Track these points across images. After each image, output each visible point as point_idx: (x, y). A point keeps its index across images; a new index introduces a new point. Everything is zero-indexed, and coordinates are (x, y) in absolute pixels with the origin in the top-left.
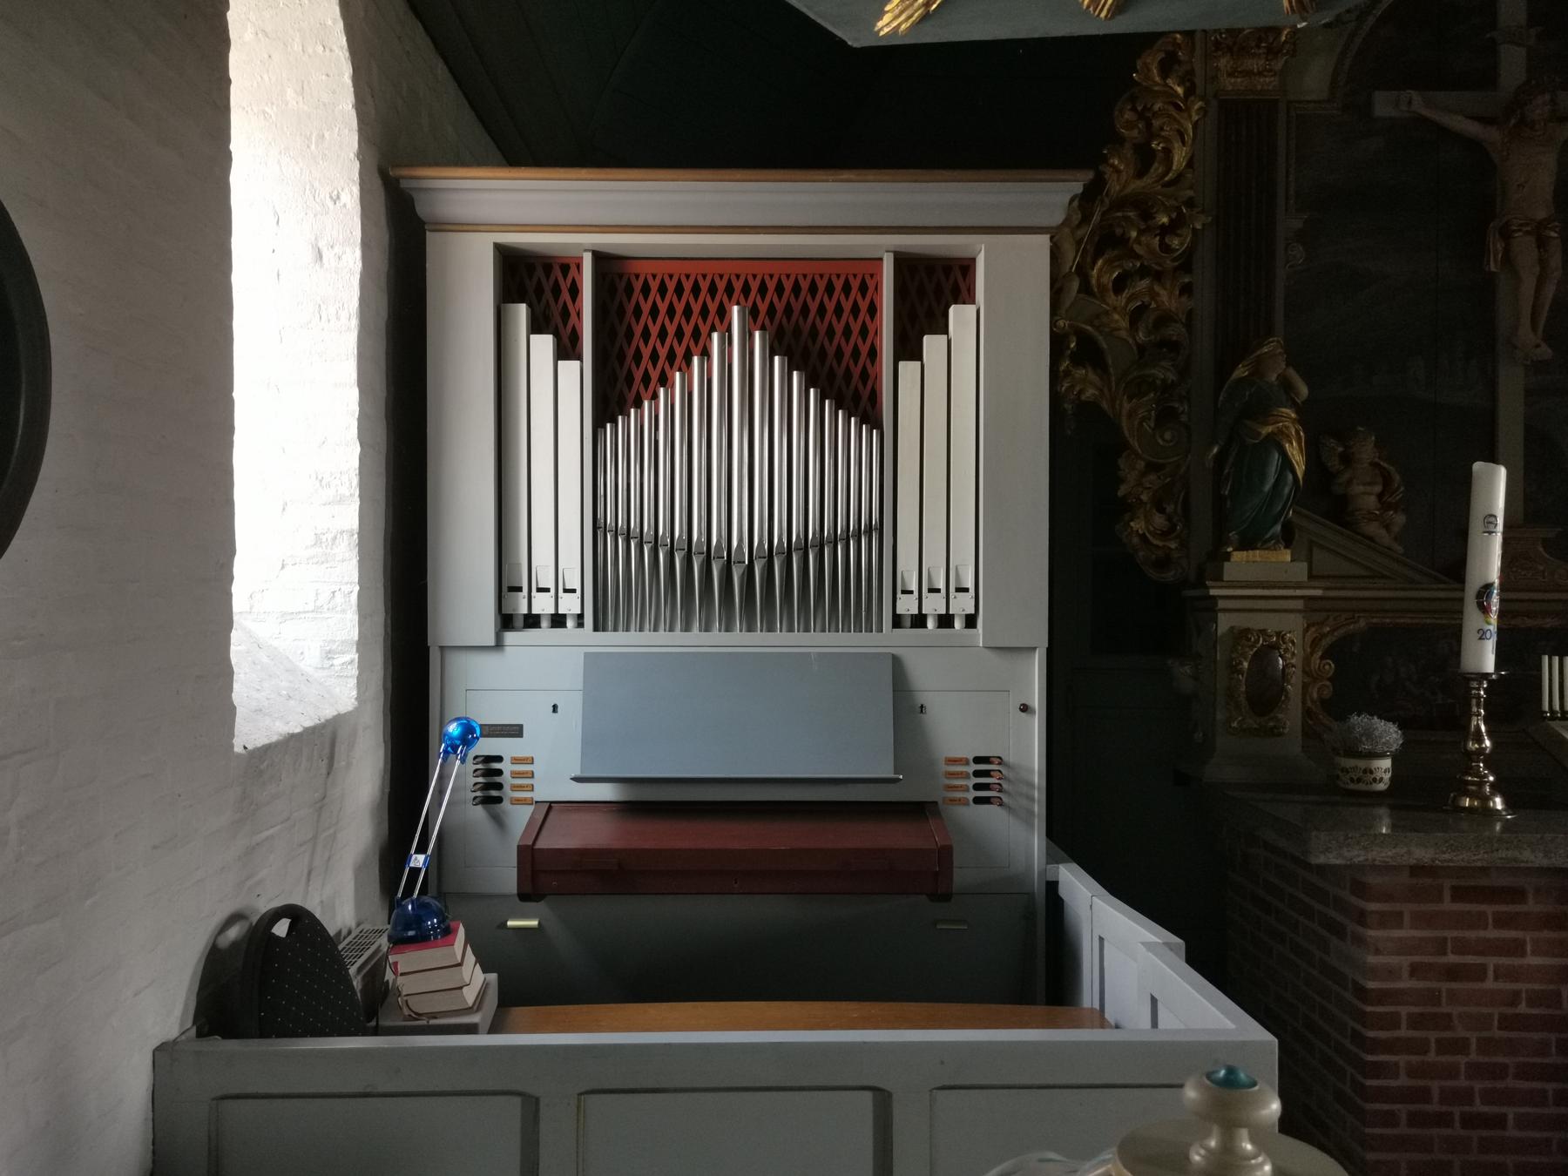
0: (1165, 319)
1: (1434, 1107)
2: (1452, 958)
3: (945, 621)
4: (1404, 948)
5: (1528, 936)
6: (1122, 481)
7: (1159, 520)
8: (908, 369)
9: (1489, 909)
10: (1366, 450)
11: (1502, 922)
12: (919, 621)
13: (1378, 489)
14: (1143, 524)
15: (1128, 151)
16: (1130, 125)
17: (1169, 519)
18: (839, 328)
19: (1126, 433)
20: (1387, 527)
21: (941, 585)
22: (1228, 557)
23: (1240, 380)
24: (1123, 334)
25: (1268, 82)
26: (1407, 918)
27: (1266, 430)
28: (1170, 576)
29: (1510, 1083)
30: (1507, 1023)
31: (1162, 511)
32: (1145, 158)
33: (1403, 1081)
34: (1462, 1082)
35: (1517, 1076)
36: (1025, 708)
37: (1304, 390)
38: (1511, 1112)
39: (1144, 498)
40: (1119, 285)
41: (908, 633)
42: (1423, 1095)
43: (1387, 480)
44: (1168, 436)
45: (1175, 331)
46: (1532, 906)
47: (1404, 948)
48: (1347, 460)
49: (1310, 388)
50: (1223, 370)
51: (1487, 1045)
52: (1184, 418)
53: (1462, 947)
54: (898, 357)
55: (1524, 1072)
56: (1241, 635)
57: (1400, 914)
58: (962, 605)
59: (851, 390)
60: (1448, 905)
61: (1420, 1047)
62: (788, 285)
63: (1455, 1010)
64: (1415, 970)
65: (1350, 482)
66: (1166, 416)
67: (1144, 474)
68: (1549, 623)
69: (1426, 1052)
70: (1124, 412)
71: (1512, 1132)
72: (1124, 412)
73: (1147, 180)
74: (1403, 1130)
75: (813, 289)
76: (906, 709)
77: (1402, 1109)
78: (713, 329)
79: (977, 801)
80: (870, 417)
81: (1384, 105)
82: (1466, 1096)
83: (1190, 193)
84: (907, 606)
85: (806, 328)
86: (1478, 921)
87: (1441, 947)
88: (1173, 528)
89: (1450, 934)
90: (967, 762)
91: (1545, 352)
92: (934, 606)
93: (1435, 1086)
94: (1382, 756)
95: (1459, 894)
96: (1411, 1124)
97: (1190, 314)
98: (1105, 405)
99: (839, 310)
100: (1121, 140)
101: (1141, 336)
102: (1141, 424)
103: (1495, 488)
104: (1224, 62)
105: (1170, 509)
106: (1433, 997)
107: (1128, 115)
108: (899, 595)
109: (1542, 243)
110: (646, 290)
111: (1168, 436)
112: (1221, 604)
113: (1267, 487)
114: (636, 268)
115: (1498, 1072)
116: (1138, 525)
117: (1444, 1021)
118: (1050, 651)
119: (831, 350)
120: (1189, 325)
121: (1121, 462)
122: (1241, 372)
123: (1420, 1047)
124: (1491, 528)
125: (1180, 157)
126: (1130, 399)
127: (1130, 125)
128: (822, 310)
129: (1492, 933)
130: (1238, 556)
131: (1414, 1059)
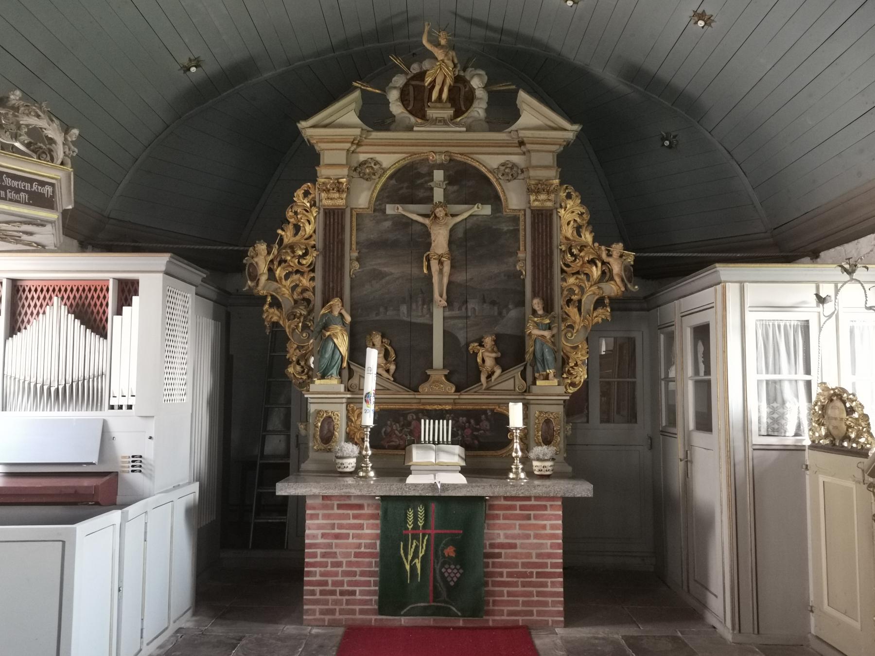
0: (305, 290)
1: (330, 588)
2: (337, 531)
4: (319, 527)
5: (365, 522)
7: (298, 368)
8: (117, 318)
9: (351, 512)
11: (355, 517)
15: (291, 226)
16: (291, 217)
17: (302, 367)
18: (98, 303)
24: (286, 296)
25: (341, 203)
26: (320, 516)
27: (328, 334)
29: (358, 578)
30: (357, 555)
32: (297, 228)
33: (318, 578)
34: (340, 578)
35: (360, 576)
38: (357, 589)
39: (294, 359)
40: (287, 277)
42: (325, 583)
45: (307, 295)
46: (366, 511)
47: (319, 527)
49: (351, 316)
51: (350, 564)
53: (341, 527)
54: (113, 315)
55: (363, 574)
56: (318, 412)
57: (318, 514)
59: (97, 325)
60: (336, 511)
61: (325, 565)
62: (81, 289)
63: (338, 551)
64: (324, 536)
68: (448, 407)
69: (327, 567)
71: (358, 597)
73: (298, 237)
74: (318, 596)
75: (90, 290)
76: (106, 436)
77: (318, 589)
78: (47, 304)
79: (133, 471)
80: (105, 337)
81: (391, 209)
82: (341, 583)
83: (313, 243)
85: (87, 303)
86: (347, 517)
87: (333, 526)
88: (303, 372)
89: (336, 522)
93: (330, 580)
94: (349, 457)
95: (340, 507)
96: (321, 594)
97: (314, 288)
98: (281, 323)
99: (99, 297)
100: (289, 222)
101: (295, 297)
104: (323, 195)
106: (330, 546)
107: (291, 214)
109: (441, 263)
110: (24, 291)
112: (310, 400)
114: (24, 283)
115: (354, 574)
116: (291, 370)
117: (334, 555)
119: (95, 311)
120: (314, 294)
123: (325, 565)
125: (309, 229)
127: (291, 217)
128: (93, 297)
129: (352, 521)
131: (322, 569)
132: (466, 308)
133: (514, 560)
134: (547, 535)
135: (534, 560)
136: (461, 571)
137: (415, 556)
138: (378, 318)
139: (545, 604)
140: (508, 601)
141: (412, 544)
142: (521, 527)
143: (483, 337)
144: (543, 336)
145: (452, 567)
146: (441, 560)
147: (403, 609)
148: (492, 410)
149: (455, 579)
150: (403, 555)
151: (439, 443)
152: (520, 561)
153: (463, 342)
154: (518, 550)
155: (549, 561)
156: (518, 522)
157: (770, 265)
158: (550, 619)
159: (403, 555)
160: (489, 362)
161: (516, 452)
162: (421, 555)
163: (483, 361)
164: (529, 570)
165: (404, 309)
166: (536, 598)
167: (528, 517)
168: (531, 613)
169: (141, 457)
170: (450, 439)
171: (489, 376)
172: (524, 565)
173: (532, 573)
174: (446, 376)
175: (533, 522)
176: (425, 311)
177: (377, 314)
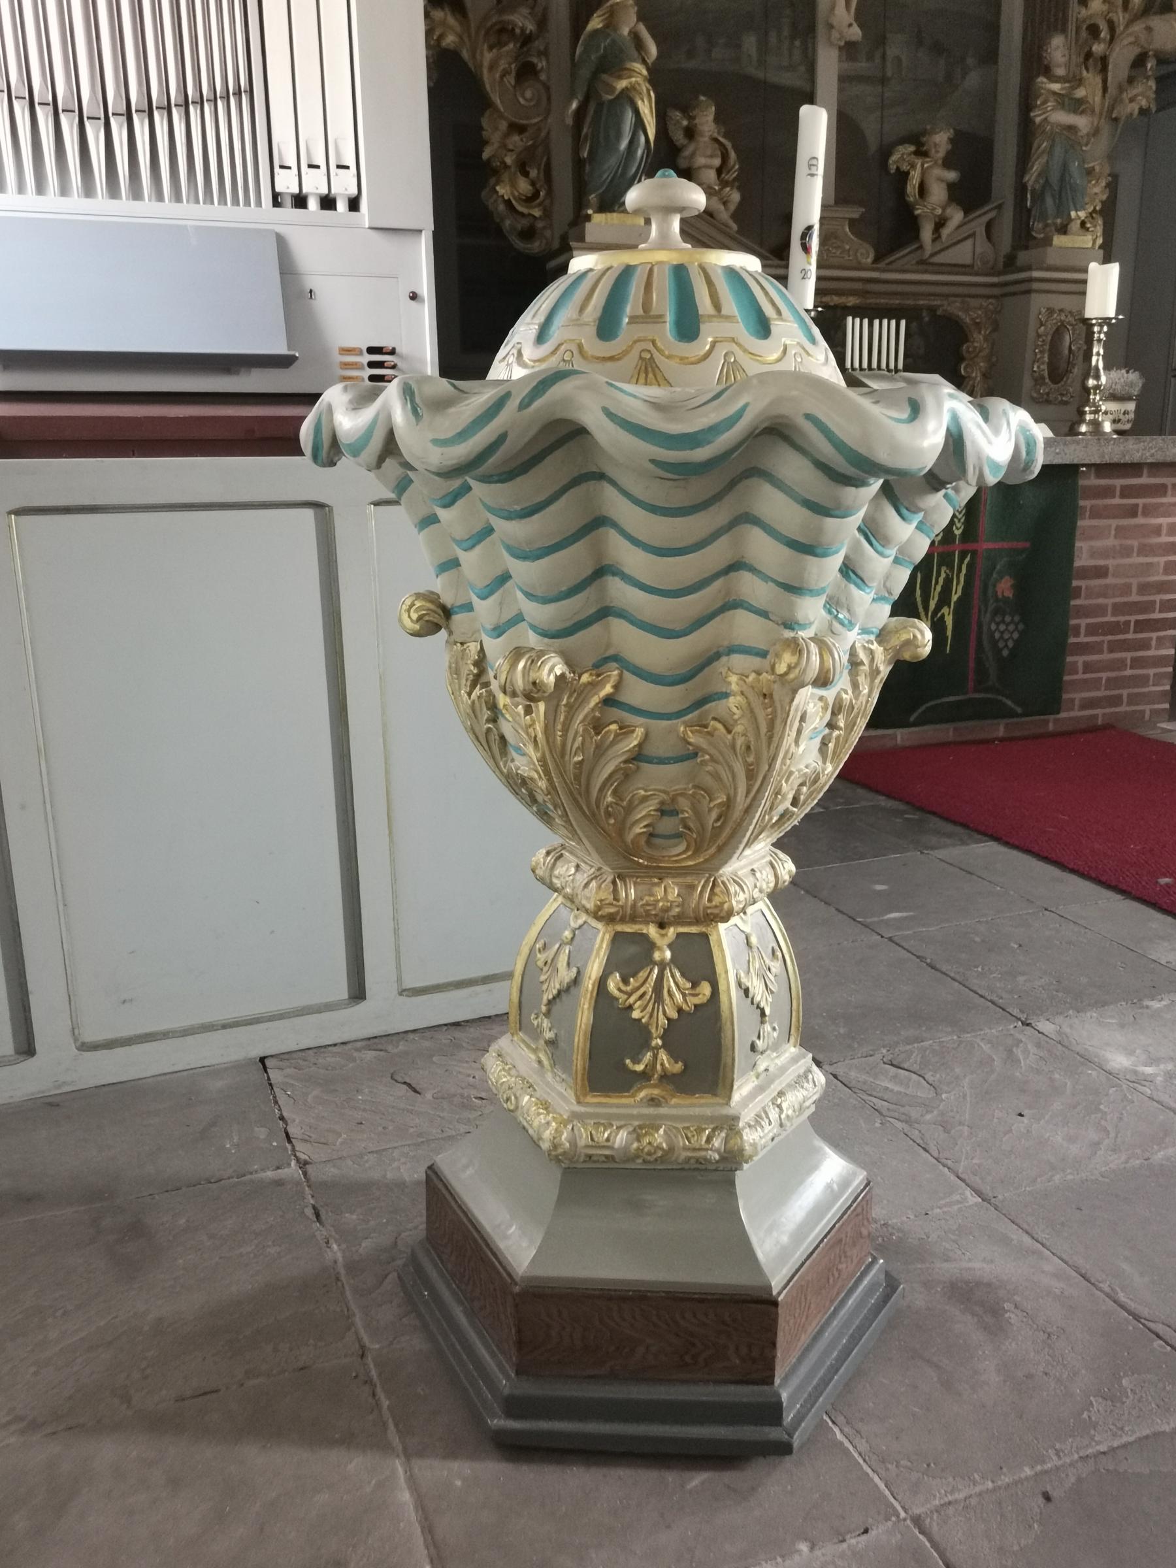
3: (328, 203)
6: (485, 143)
10: (707, 120)
12: (300, 201)
13: (717, 162)
14: (508, 188)
17: (533, 184)
19: (488, 87)
20: (725, 203)
21: (320, 160)
22: (588, 218)
23: (596, 32)
27: (622, 84)
28: (536, 247)
31: (526, 174)
36: (414, 297)
37: (653, 50)
39: (509, 160)
41: (288, 213)
43: (725, 158)
44: (528, 94)
48: (690, 133)
50: (578, 21)
52: (543, 77)
58: (344, 185)
65: (693, 154)
66: (526, 72)
67: (507, 135)
70: (486, 64)
72: (486, 64)
84: (287, 183)
88: (536, 195)
90: (360, 353)
91: (856, 33)
92: (315, 184)
98: (465, 54)
102: (502, 76)
103: (816, 128)
105: (533, 173)
108: (277, 170)
111: (528, 94)
113: (624, 145)
116: (503, 190)
118: (436, 235)
121: (485, 122)
122: (596, 23)
124: (813, 171)
126: (491, 48)
130: (598, 218)
132: (884, 57)
133: (1101, 601)
134: (1160, 545)
135: (1134, 597)
136: (1021, 627)
137: (944, 599)
138: (691, 64)
139: (1144, 680)
140: (1085, 681)
141: (938, 575)
142: (1120, 532)
143: (924, 133)
144: (1072, 128)
145: (1008, 619)
146: (992, 605)
147: (913, 710)
148: (932, 310)
149: (1010, 644)
150: (919, 599)
151: (897, 370)
152: (1110, 602)
153: (873, 144)
154: (1109, 580)
155: (1158, 598)
156: (1114, 523)
157: (267, 370)
158: (1147, 708)
159: (919, 599)
160: (938, 194)
161: (1097, 377)
162: (955, 598)
163: (923, 190)
164: (1122, 619)
165: (750, 43)
166: (1129, 672)
167: (1133, 512)
168: (1116, 701)
169: (392, 352)
170: (900, 366)
171: (940, 224)
172: (1118, 609)
173: (1128, 623)
174: (852, 223)
175: (1140, 520)
176: (797, 55)
177: (690, 54)
